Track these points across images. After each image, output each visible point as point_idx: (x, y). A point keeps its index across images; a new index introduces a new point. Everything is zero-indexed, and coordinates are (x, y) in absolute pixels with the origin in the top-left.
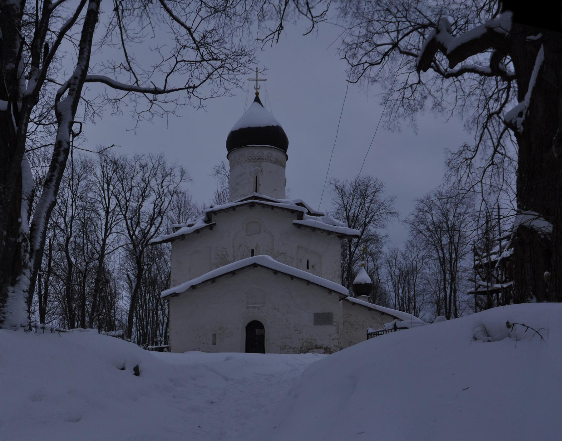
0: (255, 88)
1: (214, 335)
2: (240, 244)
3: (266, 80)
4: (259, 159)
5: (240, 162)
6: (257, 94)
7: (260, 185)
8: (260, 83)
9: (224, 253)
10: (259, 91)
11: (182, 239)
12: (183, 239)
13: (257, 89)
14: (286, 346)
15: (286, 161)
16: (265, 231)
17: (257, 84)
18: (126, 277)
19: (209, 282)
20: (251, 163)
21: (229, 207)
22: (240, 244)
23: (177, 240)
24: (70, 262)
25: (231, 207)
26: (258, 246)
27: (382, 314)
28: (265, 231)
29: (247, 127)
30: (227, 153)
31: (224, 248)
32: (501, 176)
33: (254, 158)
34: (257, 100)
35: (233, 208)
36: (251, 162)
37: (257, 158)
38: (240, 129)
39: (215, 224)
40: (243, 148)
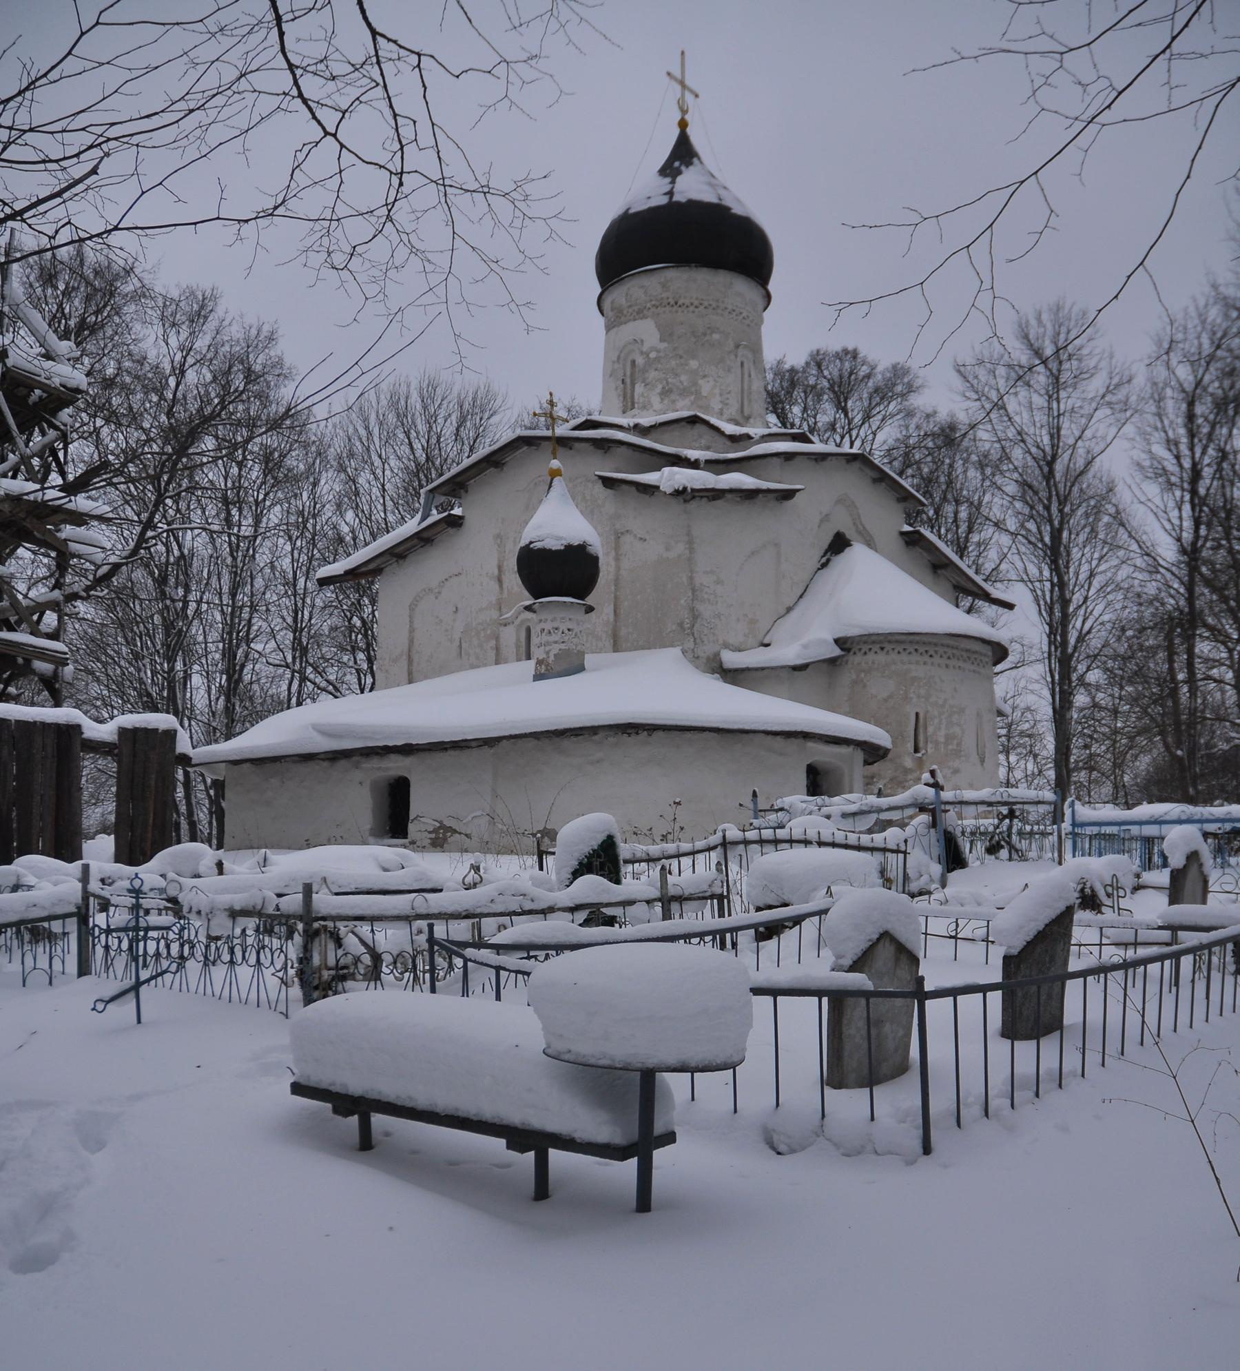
6: (683, 125)
13: (684, 111)
15: (765, 309)
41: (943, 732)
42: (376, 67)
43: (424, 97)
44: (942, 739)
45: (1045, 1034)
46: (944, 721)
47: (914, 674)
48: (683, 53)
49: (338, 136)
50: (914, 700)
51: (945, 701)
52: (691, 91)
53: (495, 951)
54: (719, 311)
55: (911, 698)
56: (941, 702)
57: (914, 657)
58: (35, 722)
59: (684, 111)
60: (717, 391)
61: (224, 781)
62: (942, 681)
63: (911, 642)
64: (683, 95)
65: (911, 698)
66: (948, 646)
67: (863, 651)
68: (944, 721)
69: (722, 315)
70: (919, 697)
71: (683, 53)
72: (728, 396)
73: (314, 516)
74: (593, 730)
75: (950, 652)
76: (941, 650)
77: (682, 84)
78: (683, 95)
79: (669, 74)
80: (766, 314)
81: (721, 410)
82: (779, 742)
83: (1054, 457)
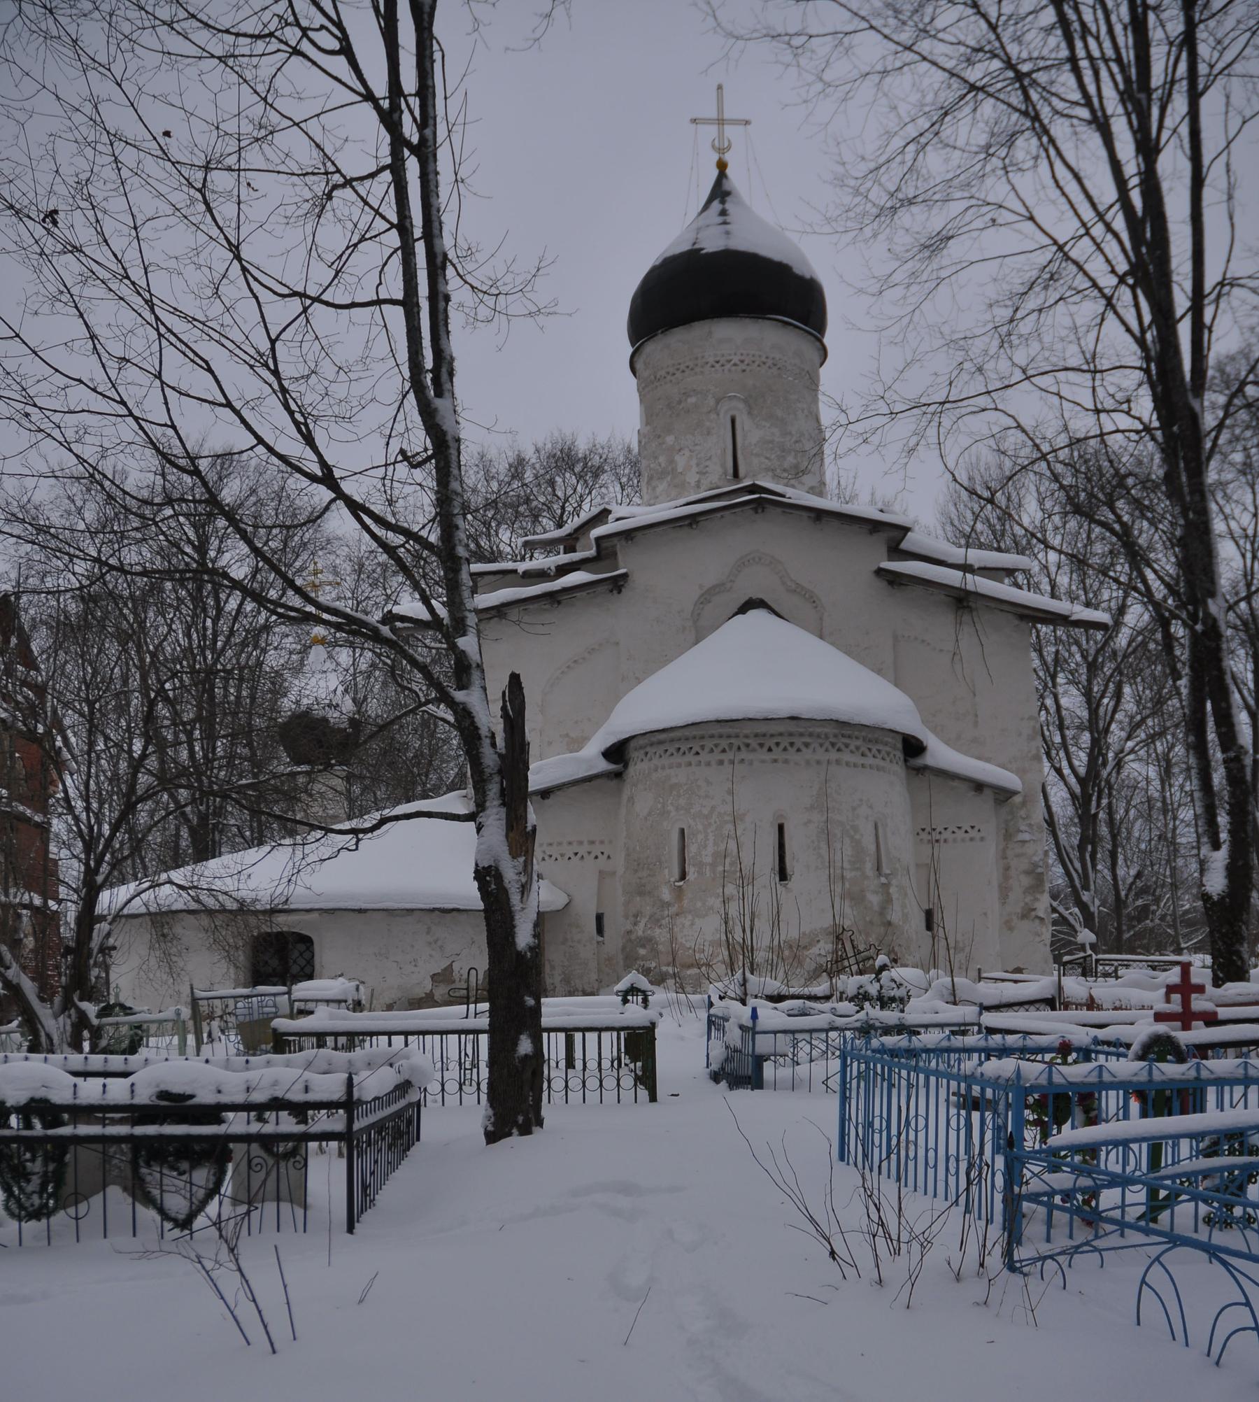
0: (713, 146)
3: (747, 123)
6: (722, 166)
8: (728, 129)
10: (728, 157)
13: (721, 150)
15: (822, 364)
17: (721, 134)
18: (1059, 795)
24: (1224, 730)
27: (543, 798)
30: (630, 350)
35: (691, 521)
39: (625, 576)
41: (710, 849)
44: (709, 860)
46: (711, 837)
47: (674, 780)
50: (673, 814)
51: (713, 808)
53: (1179, 1024)
54: (698, 370)
55: (669, 812)
56: (705, 812)
57: (678, 759)
58: (514, 927)
60: (694, 462)
62: (708, 783)
63: (672, 740)
65: (669, 812)
66: (721, 736)
67: (782, 746)
68: (711, 837)
69: (702, 373)
70: (677, 809)
72: (708, 463)
74: (410, 911)
75: (724, 743)
76: (709, 744)
80: (822, 371)
81: (699, 481)
82: (356, 915)
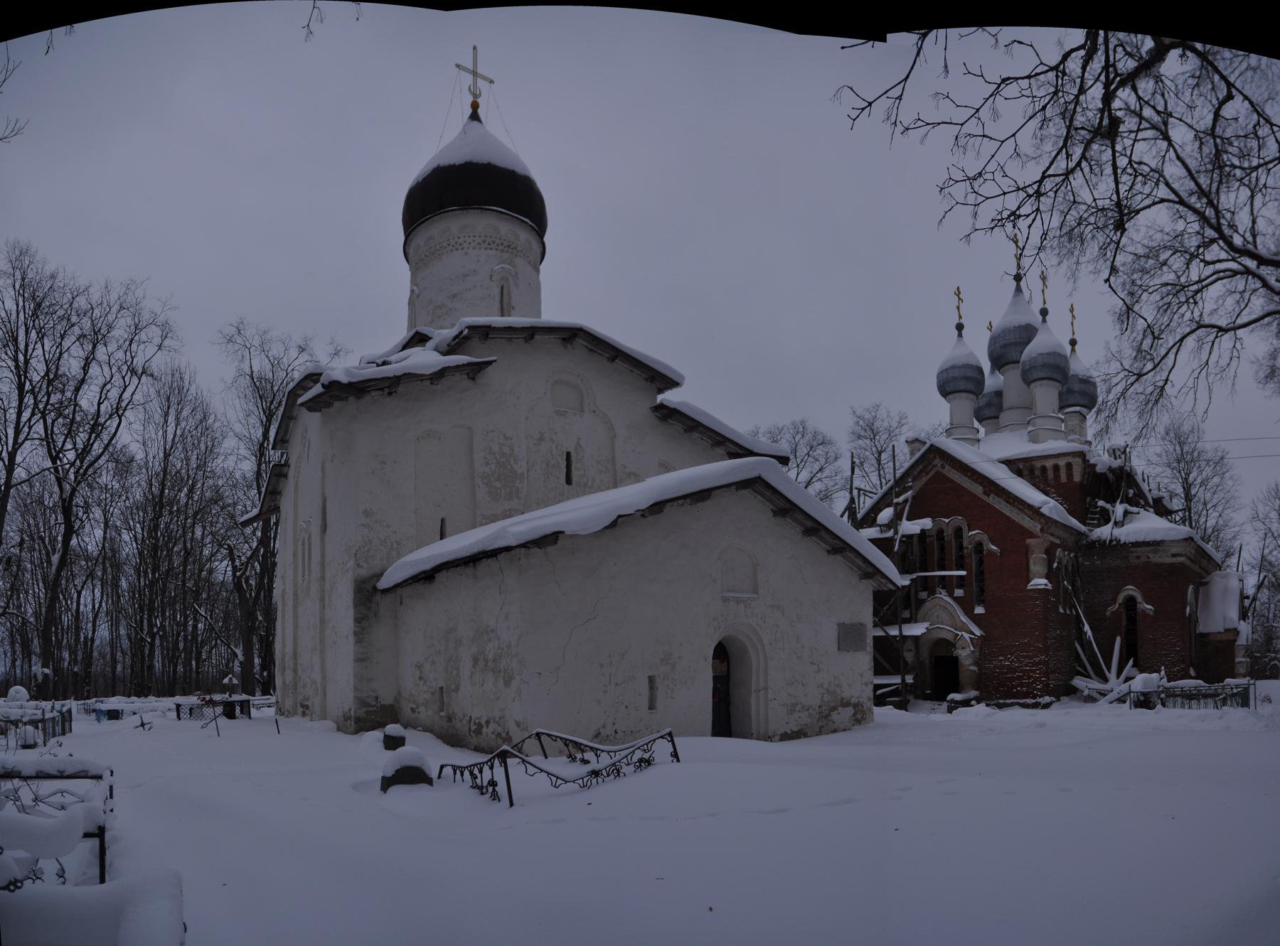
1: (651, 680)
2: (540, 433)
4: (509, 246)
5: (461, 244)
7: (513, 308)
9: (506, 450)
11: (387, 391)
12: (390, 394)
13: (476, 96)
14: (796, 704)
16: (594, 412)
19: (733, 488)
20: (493, 252)
21: (529, 326)
22: (540, 433)
23: (373, 393)
25: (523, 329)
26: (581, 447)
28: (594, 412)
29: (486, 162)
31: (506, 438)
32: (92, 536)
33: (497, 241)
34: (475, 116)
36: (491, 249)
37: (505, 244)
38: (466, 163)
40: (470, 211)
42: (1170, 378)
43: (990, 83)
45: (1136, 77)
48: (475, 48)
49: (870, 101)
52: (485, 78)
59: (476, 96)
61: (1239, 620)
64: (475, 83)
71: (475, 48)
73: (1108, 416)
77: (475, 74)
78: (475, 83)
79: (458, 66)
83: (1195, 86)
